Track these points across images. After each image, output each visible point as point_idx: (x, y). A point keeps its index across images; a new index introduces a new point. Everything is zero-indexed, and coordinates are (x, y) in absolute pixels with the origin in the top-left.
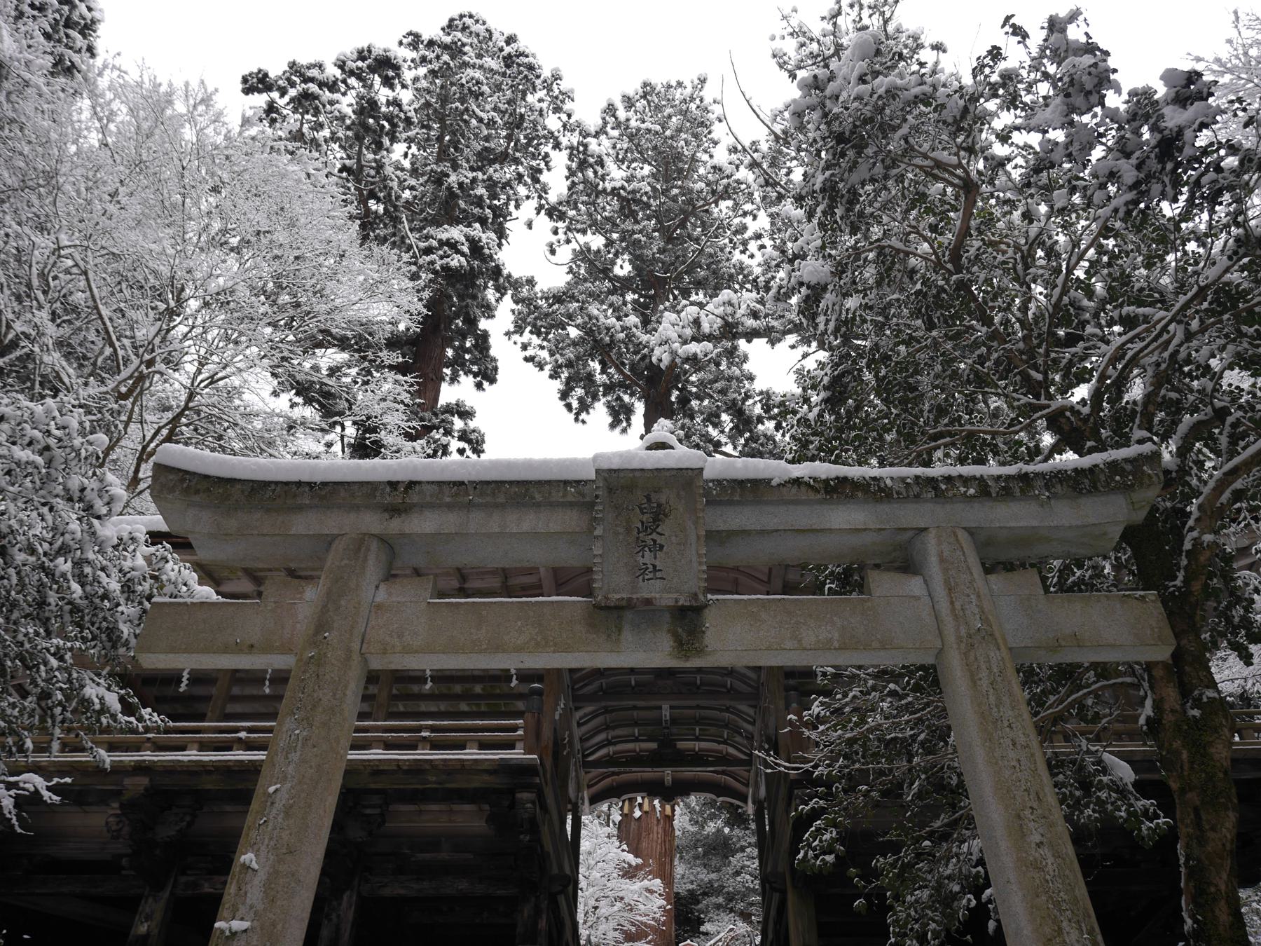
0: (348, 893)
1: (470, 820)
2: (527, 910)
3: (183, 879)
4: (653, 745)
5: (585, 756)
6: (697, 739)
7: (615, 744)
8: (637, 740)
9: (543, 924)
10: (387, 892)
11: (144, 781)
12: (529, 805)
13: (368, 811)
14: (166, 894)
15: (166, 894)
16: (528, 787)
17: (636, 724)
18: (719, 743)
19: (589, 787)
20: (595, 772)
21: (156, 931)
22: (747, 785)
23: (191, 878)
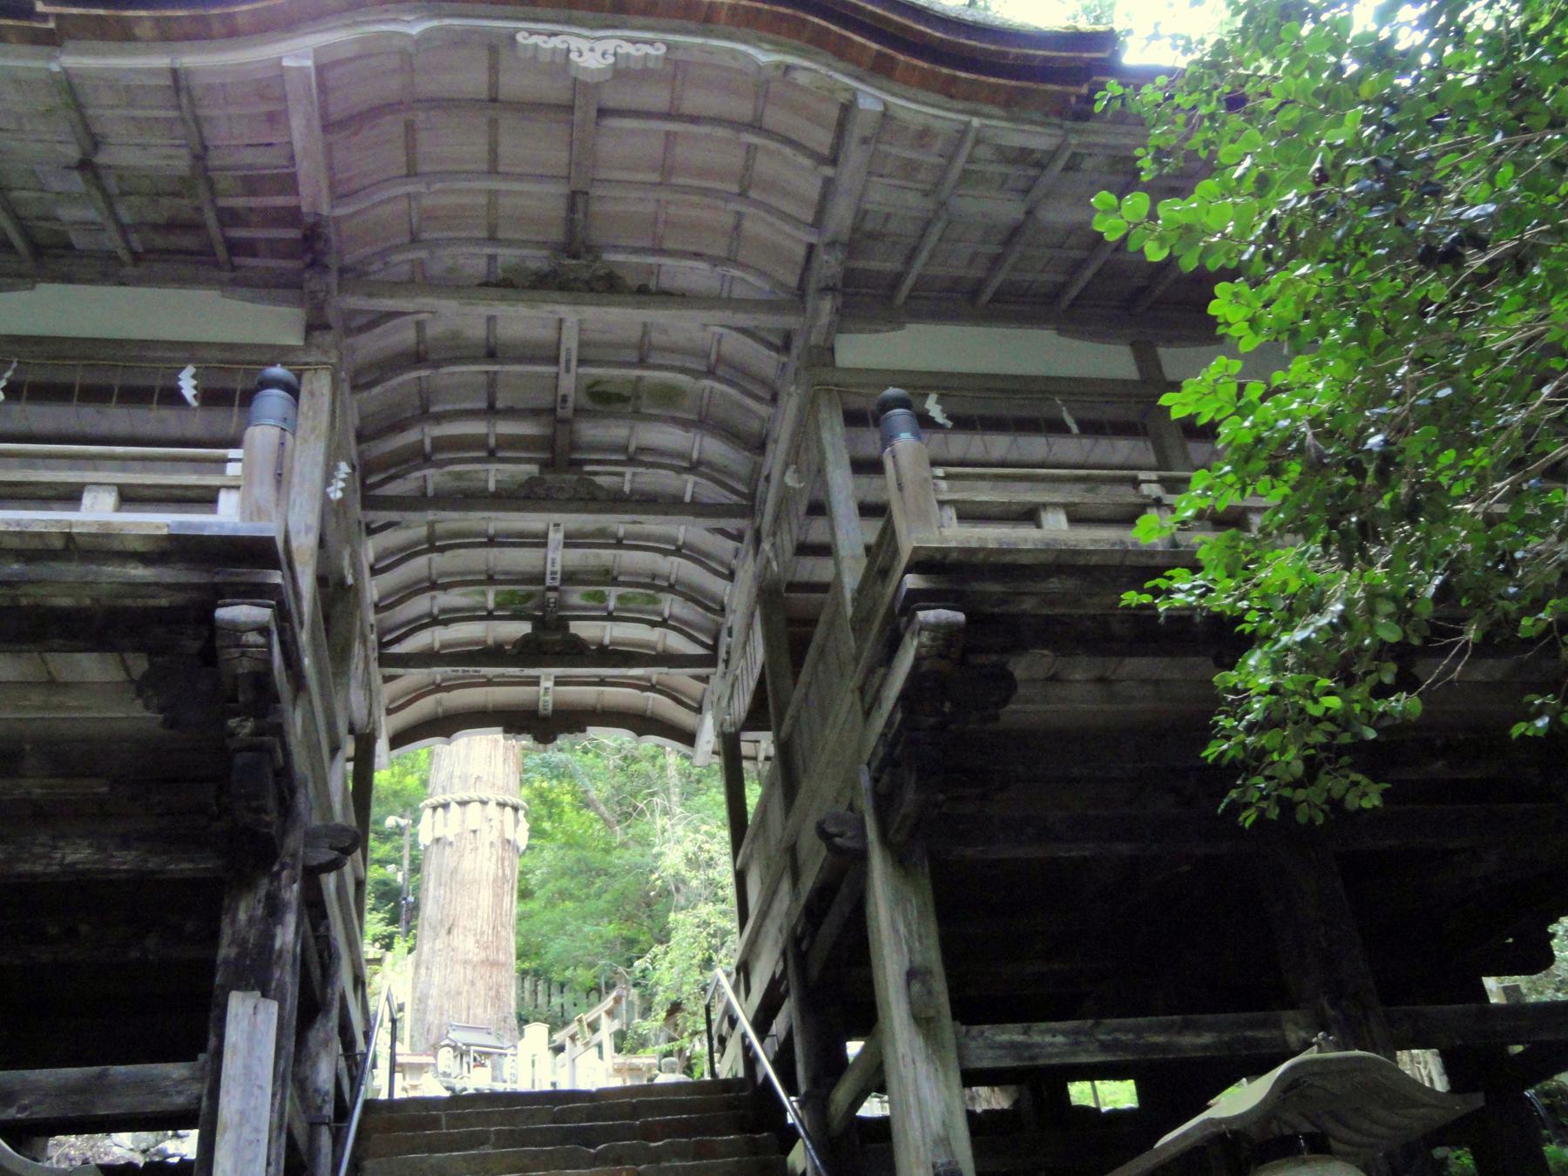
2: (246, 911)
4: (524, 628)
5: (382, 645)
6: (610, 617)
7: (446, 623)
8: (490, 616)
9: (286, 935)
12: (253, 638)
16: (254, 593)
17: (491, 580)
18: (653, 624)
22: (699, 710)
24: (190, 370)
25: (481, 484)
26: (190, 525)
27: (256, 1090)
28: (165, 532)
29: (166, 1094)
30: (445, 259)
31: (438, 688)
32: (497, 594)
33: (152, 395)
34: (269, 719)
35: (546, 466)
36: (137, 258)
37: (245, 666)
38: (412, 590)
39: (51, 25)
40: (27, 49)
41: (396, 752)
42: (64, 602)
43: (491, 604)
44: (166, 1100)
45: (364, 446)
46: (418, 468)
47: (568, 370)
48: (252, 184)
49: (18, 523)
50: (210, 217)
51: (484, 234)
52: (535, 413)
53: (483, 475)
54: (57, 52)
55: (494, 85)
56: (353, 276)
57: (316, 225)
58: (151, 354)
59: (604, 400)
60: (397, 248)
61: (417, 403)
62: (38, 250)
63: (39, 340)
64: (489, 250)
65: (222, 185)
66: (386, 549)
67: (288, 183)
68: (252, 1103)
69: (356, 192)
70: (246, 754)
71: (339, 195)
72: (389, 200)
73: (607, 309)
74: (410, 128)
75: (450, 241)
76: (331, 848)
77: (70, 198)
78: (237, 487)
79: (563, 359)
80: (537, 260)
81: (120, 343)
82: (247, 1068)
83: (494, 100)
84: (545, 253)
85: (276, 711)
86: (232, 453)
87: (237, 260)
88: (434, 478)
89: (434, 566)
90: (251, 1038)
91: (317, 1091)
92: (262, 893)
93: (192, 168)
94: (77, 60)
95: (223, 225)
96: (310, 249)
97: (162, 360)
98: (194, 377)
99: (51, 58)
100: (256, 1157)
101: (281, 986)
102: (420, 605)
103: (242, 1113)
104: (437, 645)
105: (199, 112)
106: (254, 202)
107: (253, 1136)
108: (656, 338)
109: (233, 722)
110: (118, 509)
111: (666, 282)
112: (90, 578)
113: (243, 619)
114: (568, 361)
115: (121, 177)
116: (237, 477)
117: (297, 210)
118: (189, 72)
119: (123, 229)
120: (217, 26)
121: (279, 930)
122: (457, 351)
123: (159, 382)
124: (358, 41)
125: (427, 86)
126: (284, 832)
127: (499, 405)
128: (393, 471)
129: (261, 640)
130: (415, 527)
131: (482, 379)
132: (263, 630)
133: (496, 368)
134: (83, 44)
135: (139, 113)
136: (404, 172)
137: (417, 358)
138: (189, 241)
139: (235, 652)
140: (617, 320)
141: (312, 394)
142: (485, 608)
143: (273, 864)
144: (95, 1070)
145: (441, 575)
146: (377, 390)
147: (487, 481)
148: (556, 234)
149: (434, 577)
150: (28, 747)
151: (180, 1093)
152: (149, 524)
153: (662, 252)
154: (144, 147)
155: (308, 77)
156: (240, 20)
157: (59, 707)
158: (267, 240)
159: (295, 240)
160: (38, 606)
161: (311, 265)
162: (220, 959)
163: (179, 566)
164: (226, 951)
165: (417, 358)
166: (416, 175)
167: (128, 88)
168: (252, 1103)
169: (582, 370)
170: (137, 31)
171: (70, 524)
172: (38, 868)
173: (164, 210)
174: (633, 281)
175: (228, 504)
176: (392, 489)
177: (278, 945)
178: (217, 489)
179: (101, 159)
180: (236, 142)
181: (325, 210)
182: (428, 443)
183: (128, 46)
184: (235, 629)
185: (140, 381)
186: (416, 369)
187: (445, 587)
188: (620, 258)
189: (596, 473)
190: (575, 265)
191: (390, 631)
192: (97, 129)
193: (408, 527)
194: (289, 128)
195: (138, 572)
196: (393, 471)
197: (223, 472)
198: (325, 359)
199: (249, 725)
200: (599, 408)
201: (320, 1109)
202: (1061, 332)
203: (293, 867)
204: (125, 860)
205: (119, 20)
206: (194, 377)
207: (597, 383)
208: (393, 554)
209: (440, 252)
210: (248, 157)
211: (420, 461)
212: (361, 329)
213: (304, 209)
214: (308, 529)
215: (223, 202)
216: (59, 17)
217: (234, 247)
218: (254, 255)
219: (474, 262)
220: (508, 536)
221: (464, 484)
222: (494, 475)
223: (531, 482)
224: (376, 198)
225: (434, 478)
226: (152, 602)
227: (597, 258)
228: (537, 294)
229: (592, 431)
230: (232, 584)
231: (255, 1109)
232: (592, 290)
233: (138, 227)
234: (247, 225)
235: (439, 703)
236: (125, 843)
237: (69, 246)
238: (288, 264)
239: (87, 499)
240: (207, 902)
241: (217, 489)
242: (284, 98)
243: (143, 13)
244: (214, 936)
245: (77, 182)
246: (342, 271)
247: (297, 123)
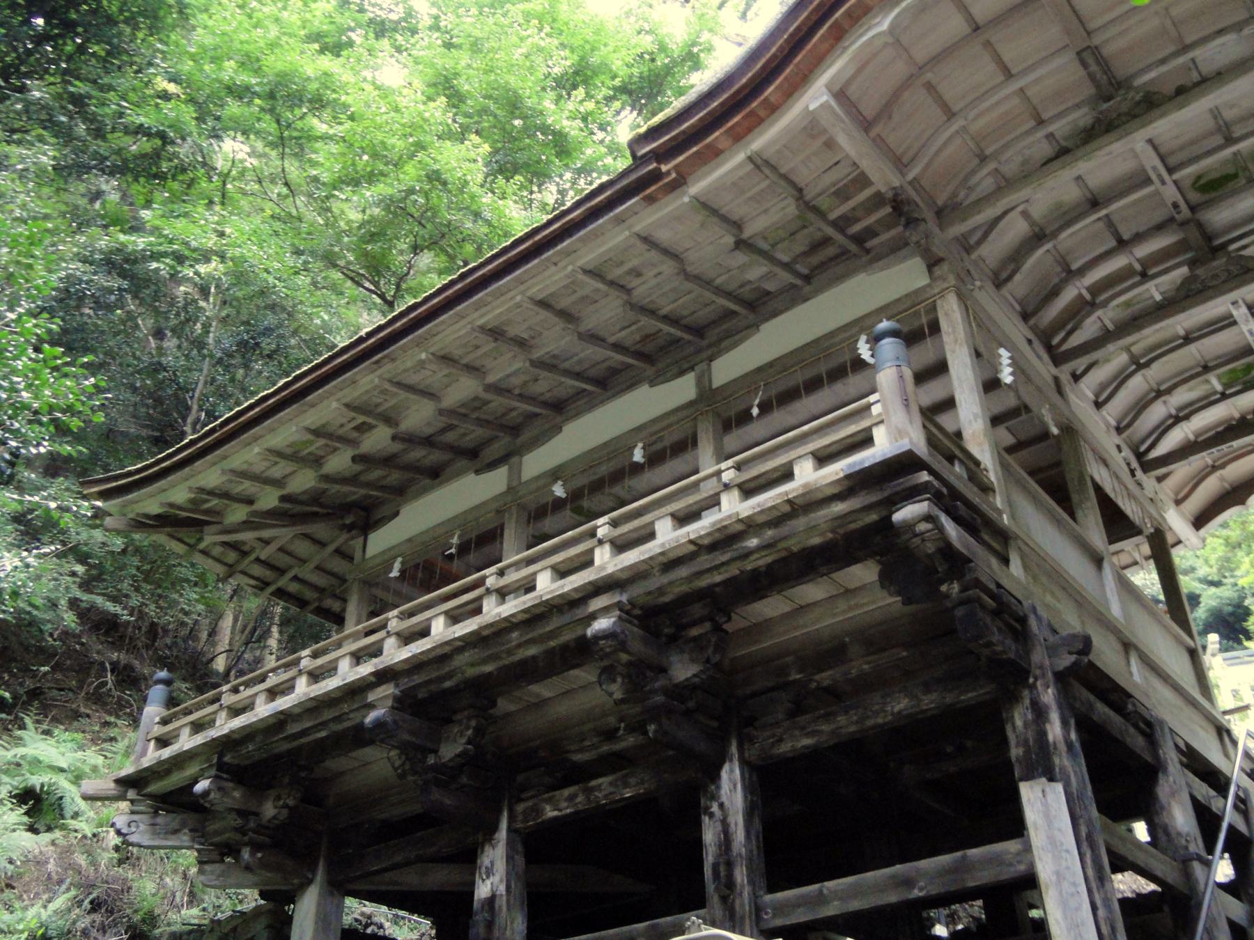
0: (726, 767)
1: (858, 594)
2: (1020, 718)
3: (520, 807)
7: (1187, 417)
8: (1224, 396)
10: (785, 748)
11: (387, 691)
12: (923, 527)
13: (694, 632)
14: (502, 834)
15: (502, 834)
16: (912, 494)
17: (1206, 369)
19: (1178, 502)
20: (1182, 471)
21: (502, 889)
23: (530, 803)
24: (863, 338)
25: (1150, 302)
26: (855, 464)
27: (1064, 854)
28: (841, 475)
29: (1011, 865)
30: (1011, 164)
31: (1214, 468)
32: (1219, 377)
33: (805, 389)
34: (968, 577)
35: (1192, 264)
36: (807, 279)
37: (930, 548)
38: (1141, 406)
39: (674, 175)
40: (671, 196)
41: (1203, 531)
42: (816, 541)
43: (1219, 388)
44: (1012, 869)
45: (1032, 322)
46: (1089, 315)
47: (1163, 183)
48: (842, 194)
49: (759, 505)
50: (830, 231)
51: (1032, 123)
52: (1160, 228)
53: (1147, 295)
54: (684, 187)
55: (970, 18)
56: (943, 214)
57: (896, 195)
58: (837, 339)
59: (1215, 187)
60: (973, 172)
61: (1059, 269)
62: (751, 305)
63: (771, 364)
64: (1041, 134)
65: (824, 207)
66: (1101, 384)
67: (862, 181)
68: (1064, 864)
69: (916, 154)
70: (961, 608)
71: (900, 164)
72: (945, 144)
73: (1155, 125)
74: (930, 87)
75: (1006, 146)
76: (1070, 653)
77: (743, 268)
78: (882, 422)
79: (1154, 177)
80: (1083, 117)
81: (816, 342)
82: (1052, 840)
83: (977, 28)
84: (1085, 110)
85: (970, 570)
86: (872, 398)
87: (869, 244)
88: (1107, 316)
89: (1149, 378)
90: (1047, 816)
91: (1179, 834)
92: (1027, 702)
93: (798, 207)
94: (698, 187)
95: (842, 231)
96: (900, 215)
97: (843, 341)
98: (867, 342)
99: (684, 193)
100: (1080, 905)
101: (1062, 769)
102: (1157, 412)
103: (1058, 873)
104: (1192, 437)
105: (783, 171)
106: (851, 204)
107: (1072, 890)
108: (1228, 115)
109: (944, 588)
110: (816, 469)
111: (1206, 69)
112: (813, 523)
113: (909, 516)
114: (1159, 176)
115: (765, 238)
116: (880, 415)
117: (878, 194)
118: (758, 154)
119: (786, 266)
120: (762, 113)
121: (1048, 727)
122: (1068, 216)
123: (847, 357)
124: (851, 60)
125: (921, 53)
126: (1028, 653)
127: (1126, 237)
128: (1069, 327)
129: (929, 526)
130: (1115, 359)
131: (1101, 224)
132: (928, 518)
133: (1103, 212)
134: (699, 173)
135: (748, 195)
136: (945, 118)
137: (1038, 237)
138: (831, 251)
139: (917, 541)
140: (1178, 124)
141: (946, 314)
142: (1215, 393)
143: (1027, 679)
144: (959, 854)
145: (1159, 384)
146: (1018, 277)
147: (1152, 297)
148: (1089, 90)
149: (1155, 387)
150: (847, 639)
151: (1019, 862)
152: (830, 474)
153: (1186, 48)
154: (766, 211)
155: (830, 107)
156: (772, 99)
157: (857, 606)
158: (877, 221)
159: (890, 214)
160: (804, 549)
161: (907, 225)
162: (1013, 759)
163: (863, 493)
164: (1015, 752)
165: (1038, 237)
166: (954, 115)
167: (734, 184)
168: (1064, 864)
169: (1176, 176)
170: (720, 147)
171: (787, 493)
172: (880, 721)
173: (800, 246)
174: (1169, 89)
175: (879, 434)
176: (1076, 340)
177: (1051, 738)
178: (869, 429)
179: (746, 234)
180: (815, 175)
181: (896, 183)
182: (1084, 292)
183: (721, 157)
184: (909, 526)
185: (833, 363)
186: (1039, 247)
187: (1169, 391)
188: (1152, 75)
189: (1245, 247)
190: (1117, 102)
191: (1143, 441)
192: (735, 217)
193: (1107, 361)
194: (841, 147)
195: (839, 508)
196: (1069, 327)
197: (870, 415)
198: (946, 285)
199: (956, 587)
200: (1213, 195)
201: (1186, 848)
202: (653, 383)
203: (1043, 675)
204: (930, 701)
205: (708, 146)
206: (867, 342)
207: (1199, 178)
208: (1111, 382)
209: (1003, 158)
210: (829, 179)
211: (1088, 308)
212: (979, 242)
213: (883, 190)
214: (976, 416)
215: (833, 216)
216: (676, 167)
217: (859, 239)
218: (876, 235)
219: (1039, 147)
220: (1200, 329)
221: (1137, 308)
222: (1155, 290)
223: (1186, 281)
224: (934, 149)
225: (1107, 316)
226: (853, 526)
227: (1130, 88)
228: (1088, 148)
229: (1221, 216)
230: (897, 493)
231: (1068, 868)
232: (1135, 117)
233: (795, 260)
234: (858, 220)
235: (1222, 479)
236: (927, 689)
237: (769, 293)
238: (893, 232)
239: (797, 470)
240: (990, 722)
241: (869, 429)
242: (825, 131)
243: (717, 134)
244: (1005, 741)
245: (741, 258)
246: (940, 213)
247: (842, 140)
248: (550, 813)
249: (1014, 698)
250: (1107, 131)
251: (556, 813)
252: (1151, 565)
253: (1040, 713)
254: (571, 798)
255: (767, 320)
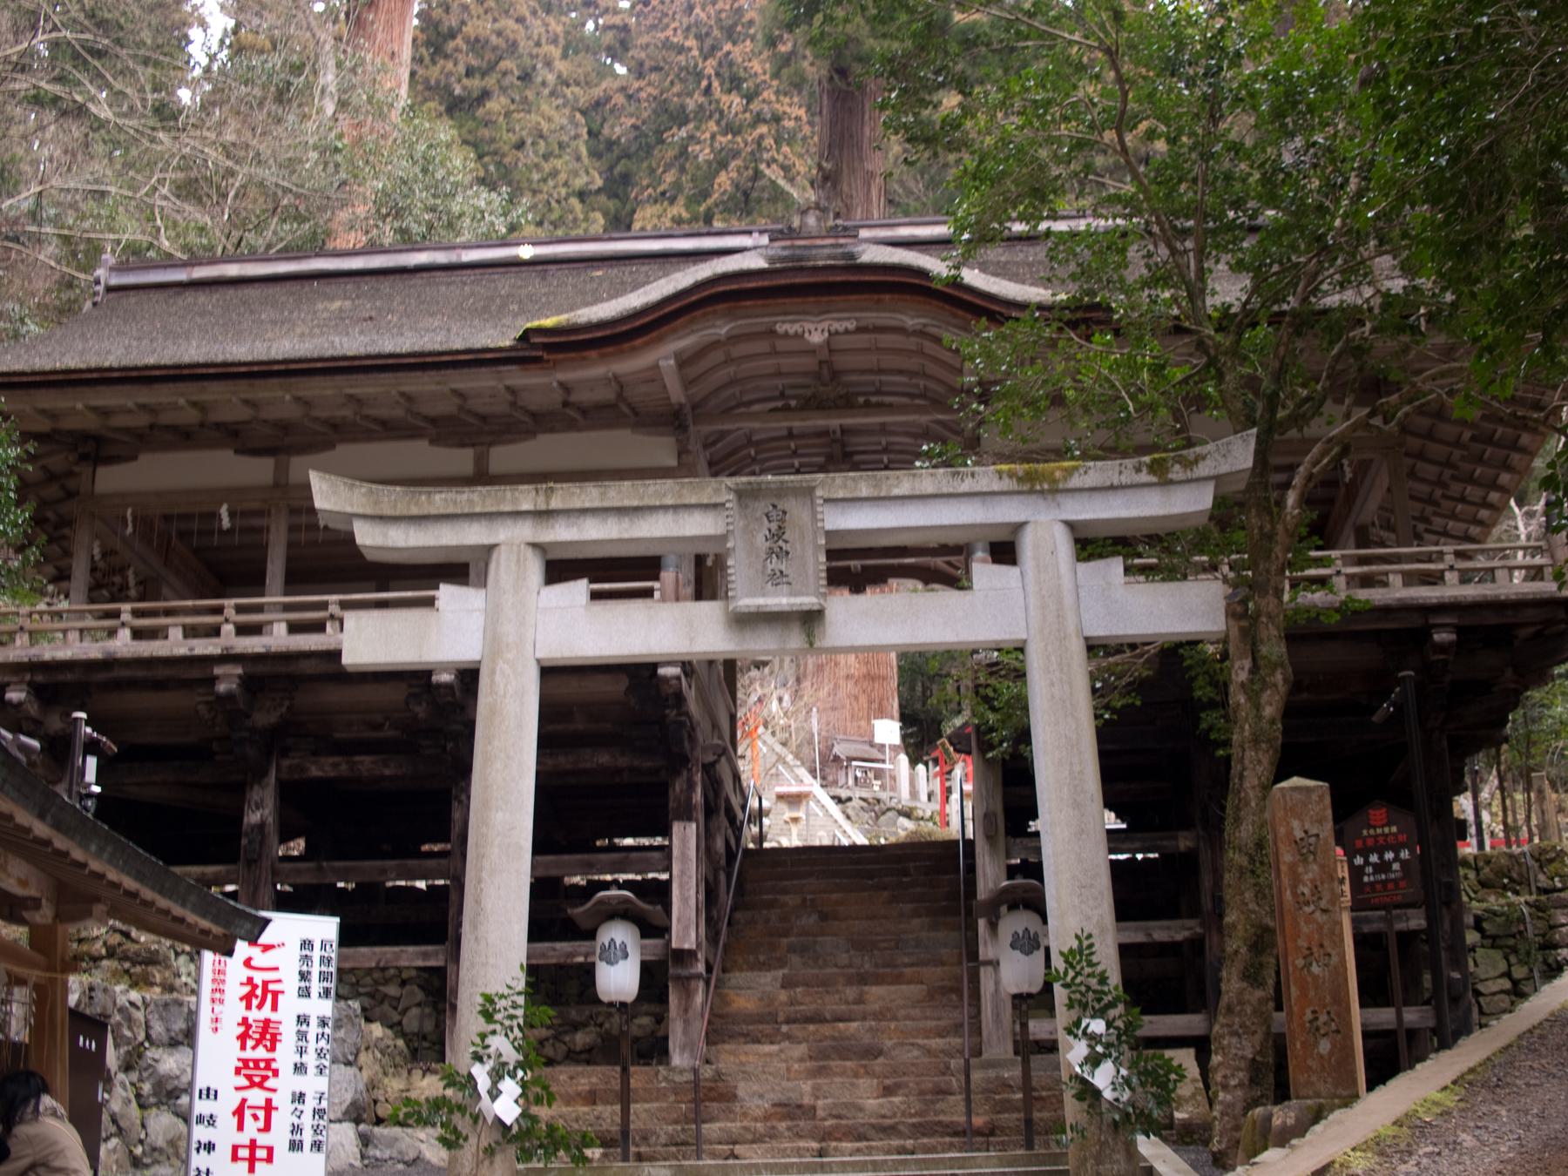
2: (678, 786)
3: (286, 763)
132: (678, 678)
184: (666, 679)
202: (433, 442)
248: (315, 772)
249: (678, 773)
250: (818, 408)
251: (320, 774)
252: (1034, 1084)
253: (691, 786)
254: (335, 765)
255: (545, 431)
